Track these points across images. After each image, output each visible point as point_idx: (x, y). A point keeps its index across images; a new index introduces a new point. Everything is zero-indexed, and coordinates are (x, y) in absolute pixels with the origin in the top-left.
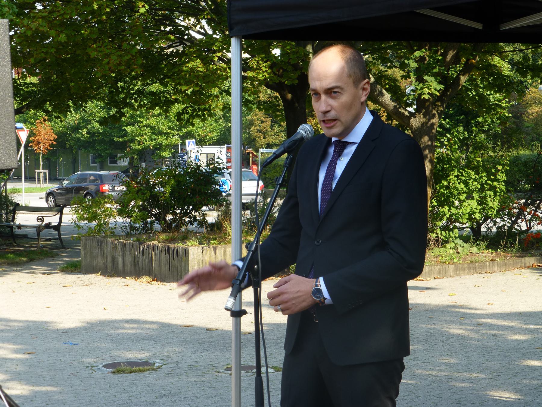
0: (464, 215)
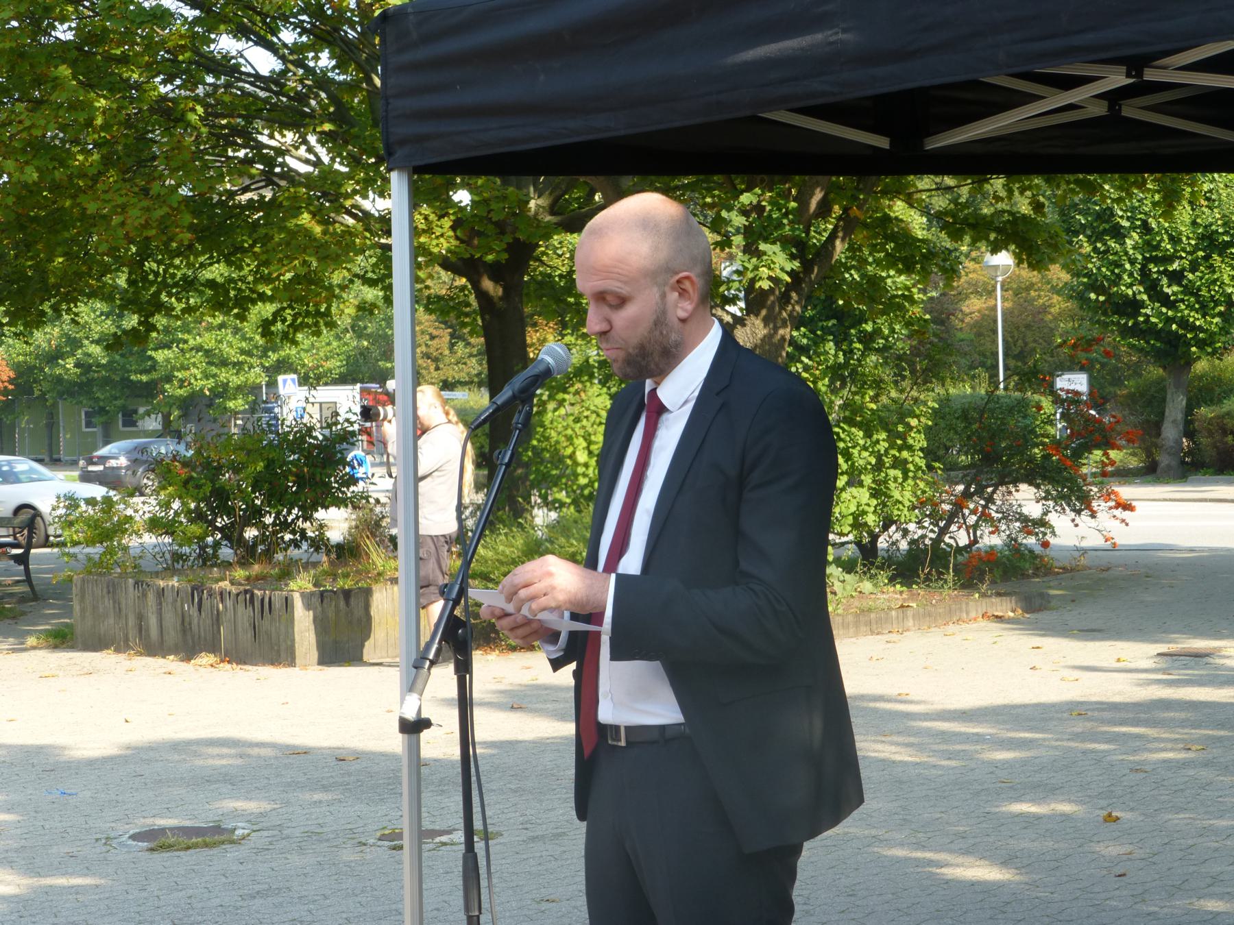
0: (843, 517)
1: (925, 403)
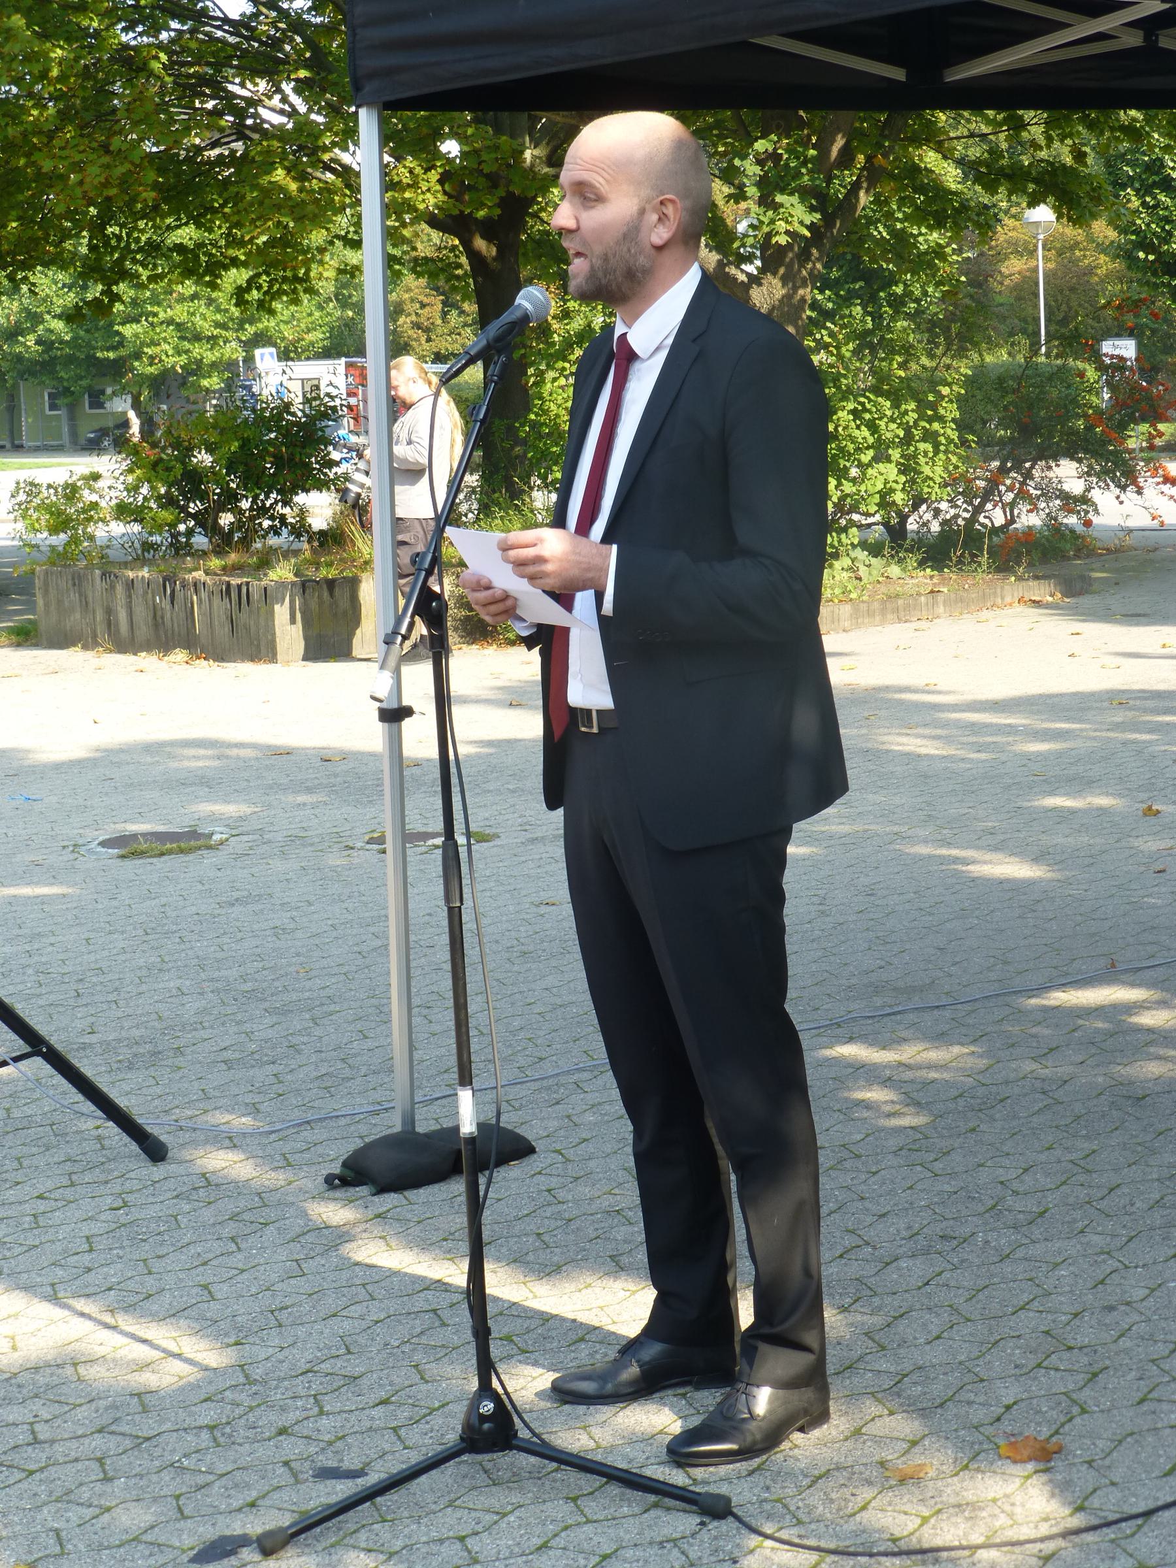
1: (957, 370)
